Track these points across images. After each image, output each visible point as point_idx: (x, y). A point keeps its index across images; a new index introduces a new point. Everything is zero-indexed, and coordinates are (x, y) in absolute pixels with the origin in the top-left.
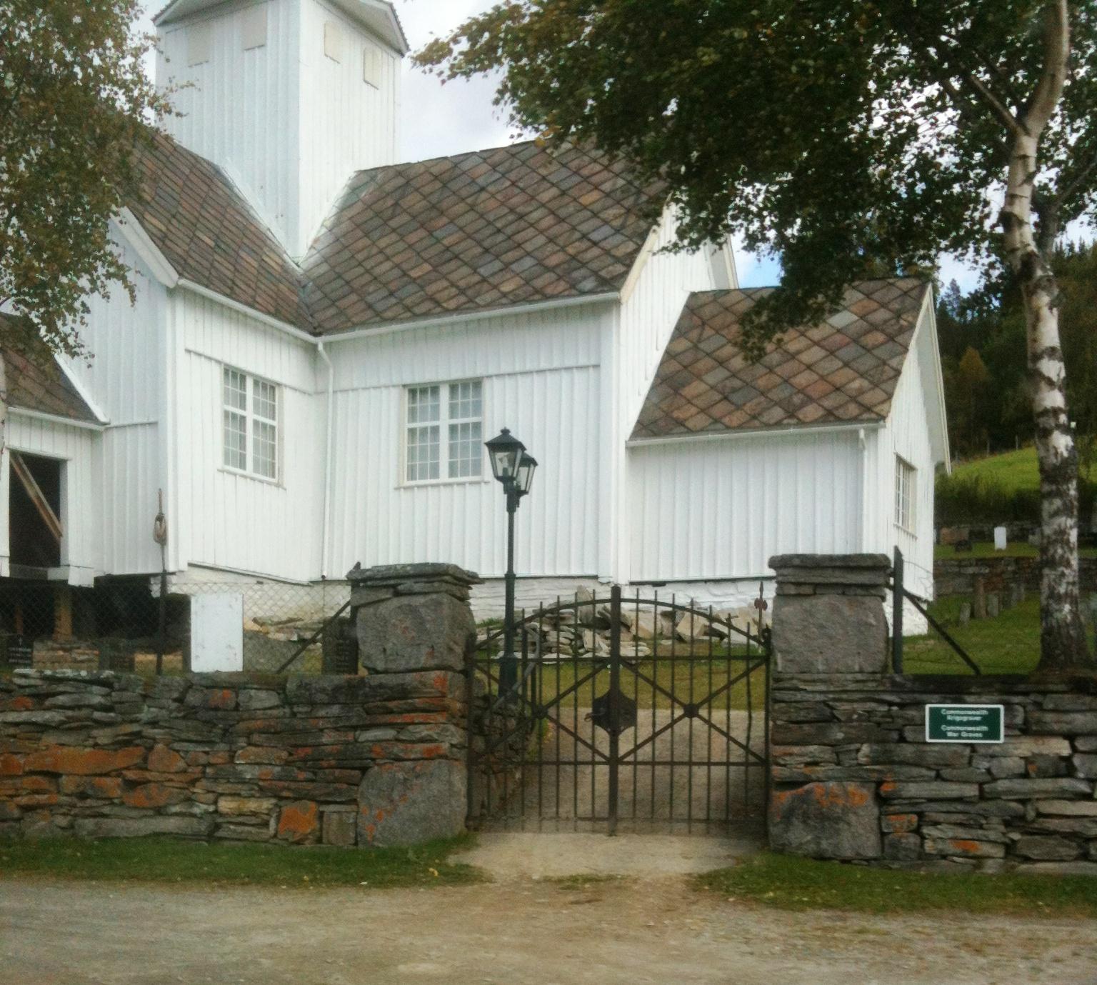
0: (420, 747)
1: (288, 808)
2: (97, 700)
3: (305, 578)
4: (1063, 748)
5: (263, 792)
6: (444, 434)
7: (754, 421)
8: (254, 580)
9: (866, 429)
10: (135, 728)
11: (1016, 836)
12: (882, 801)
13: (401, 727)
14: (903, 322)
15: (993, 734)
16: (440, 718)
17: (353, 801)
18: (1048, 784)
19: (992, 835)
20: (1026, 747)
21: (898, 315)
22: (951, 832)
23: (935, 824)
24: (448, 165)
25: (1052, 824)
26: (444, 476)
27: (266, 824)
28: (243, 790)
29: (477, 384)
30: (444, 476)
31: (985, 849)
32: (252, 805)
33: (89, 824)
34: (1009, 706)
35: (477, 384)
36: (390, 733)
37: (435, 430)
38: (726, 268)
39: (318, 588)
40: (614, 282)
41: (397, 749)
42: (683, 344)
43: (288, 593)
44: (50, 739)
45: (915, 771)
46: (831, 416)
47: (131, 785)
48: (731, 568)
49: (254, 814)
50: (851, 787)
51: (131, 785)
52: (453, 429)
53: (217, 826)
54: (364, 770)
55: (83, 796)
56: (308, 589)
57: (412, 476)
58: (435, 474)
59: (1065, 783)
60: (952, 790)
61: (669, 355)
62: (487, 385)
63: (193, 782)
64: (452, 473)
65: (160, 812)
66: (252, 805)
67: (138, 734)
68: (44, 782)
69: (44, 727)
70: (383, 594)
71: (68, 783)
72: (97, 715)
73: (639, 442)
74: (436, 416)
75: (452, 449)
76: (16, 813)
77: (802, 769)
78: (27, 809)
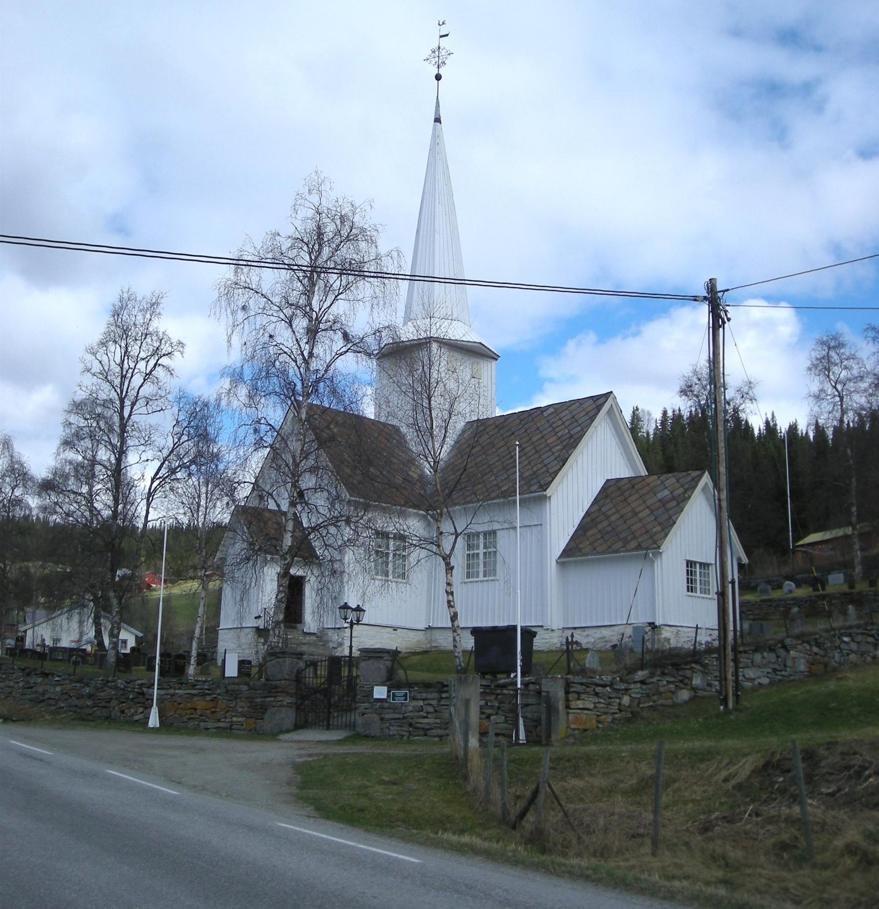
0: (279, 703)
1: (249, 720)
2: (206, 687)
3: (422, 627)
4: (421, 703)
5: (244, 715)
6: (481, 556)
7: (609, 550)
8: (392, 629)
9: (652, 553)
10: (215, 696)
11: (411, 729)
12: (382, 719)
13: (275, 697)
14: (686, 495)
15: (406, 700)
16: (284, 694)
17: (262, 719)
18: (417, 714)
19: (405, 729)
20: (414, 703)
21: (685, 492)
22: (396, 728)
23: (393, 726)
24: (503, 419)
25: (419, 725)
26: (481, 578)
27: (243, 725)
28: (238, 714)
29: (494, 533)
30: (481, 578)
31: (403, 733)
32: (240, 719)
33: (202, 724)
34: (410, 692)
35: (494, 533)
36: (272, 699)
37: (478, 554)
38: (635, 461)
39: (429, 632)
40: (545, 486)
41: (274, 704)
42: (596, 507)
43: (412, 634)
44: (195, 699)
45: (388, 710)
46: (639, 547)
47: (213, 712)
48: (568, 624)
49: (240, 722)
50: (374, 715)
51: (213, 712)
52: (485, 553)
53: (232, 725)
54: (267, 709)
55: (201, 715)
56: (423, 632)
57: (468, 577)
58: (478, 577)
59: (421, 713)
60: (397, 716)
61: (588, 514)
62: (498, 533)
63: (227, 712)
64: (485, 576)
65: (219, 721)
66: (240, 719)
67: (215, 698)
68: (193, 711)
69: (194, 695)
70: (273, 658)
71: (199, 712)
72: (207, 691)
73: (562, 560)
74: (478, 548)
75: (485, 563)
76: (186, 720)
77: (363, 710)
78: (189, 719)
